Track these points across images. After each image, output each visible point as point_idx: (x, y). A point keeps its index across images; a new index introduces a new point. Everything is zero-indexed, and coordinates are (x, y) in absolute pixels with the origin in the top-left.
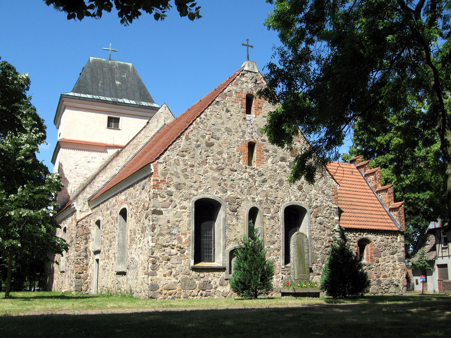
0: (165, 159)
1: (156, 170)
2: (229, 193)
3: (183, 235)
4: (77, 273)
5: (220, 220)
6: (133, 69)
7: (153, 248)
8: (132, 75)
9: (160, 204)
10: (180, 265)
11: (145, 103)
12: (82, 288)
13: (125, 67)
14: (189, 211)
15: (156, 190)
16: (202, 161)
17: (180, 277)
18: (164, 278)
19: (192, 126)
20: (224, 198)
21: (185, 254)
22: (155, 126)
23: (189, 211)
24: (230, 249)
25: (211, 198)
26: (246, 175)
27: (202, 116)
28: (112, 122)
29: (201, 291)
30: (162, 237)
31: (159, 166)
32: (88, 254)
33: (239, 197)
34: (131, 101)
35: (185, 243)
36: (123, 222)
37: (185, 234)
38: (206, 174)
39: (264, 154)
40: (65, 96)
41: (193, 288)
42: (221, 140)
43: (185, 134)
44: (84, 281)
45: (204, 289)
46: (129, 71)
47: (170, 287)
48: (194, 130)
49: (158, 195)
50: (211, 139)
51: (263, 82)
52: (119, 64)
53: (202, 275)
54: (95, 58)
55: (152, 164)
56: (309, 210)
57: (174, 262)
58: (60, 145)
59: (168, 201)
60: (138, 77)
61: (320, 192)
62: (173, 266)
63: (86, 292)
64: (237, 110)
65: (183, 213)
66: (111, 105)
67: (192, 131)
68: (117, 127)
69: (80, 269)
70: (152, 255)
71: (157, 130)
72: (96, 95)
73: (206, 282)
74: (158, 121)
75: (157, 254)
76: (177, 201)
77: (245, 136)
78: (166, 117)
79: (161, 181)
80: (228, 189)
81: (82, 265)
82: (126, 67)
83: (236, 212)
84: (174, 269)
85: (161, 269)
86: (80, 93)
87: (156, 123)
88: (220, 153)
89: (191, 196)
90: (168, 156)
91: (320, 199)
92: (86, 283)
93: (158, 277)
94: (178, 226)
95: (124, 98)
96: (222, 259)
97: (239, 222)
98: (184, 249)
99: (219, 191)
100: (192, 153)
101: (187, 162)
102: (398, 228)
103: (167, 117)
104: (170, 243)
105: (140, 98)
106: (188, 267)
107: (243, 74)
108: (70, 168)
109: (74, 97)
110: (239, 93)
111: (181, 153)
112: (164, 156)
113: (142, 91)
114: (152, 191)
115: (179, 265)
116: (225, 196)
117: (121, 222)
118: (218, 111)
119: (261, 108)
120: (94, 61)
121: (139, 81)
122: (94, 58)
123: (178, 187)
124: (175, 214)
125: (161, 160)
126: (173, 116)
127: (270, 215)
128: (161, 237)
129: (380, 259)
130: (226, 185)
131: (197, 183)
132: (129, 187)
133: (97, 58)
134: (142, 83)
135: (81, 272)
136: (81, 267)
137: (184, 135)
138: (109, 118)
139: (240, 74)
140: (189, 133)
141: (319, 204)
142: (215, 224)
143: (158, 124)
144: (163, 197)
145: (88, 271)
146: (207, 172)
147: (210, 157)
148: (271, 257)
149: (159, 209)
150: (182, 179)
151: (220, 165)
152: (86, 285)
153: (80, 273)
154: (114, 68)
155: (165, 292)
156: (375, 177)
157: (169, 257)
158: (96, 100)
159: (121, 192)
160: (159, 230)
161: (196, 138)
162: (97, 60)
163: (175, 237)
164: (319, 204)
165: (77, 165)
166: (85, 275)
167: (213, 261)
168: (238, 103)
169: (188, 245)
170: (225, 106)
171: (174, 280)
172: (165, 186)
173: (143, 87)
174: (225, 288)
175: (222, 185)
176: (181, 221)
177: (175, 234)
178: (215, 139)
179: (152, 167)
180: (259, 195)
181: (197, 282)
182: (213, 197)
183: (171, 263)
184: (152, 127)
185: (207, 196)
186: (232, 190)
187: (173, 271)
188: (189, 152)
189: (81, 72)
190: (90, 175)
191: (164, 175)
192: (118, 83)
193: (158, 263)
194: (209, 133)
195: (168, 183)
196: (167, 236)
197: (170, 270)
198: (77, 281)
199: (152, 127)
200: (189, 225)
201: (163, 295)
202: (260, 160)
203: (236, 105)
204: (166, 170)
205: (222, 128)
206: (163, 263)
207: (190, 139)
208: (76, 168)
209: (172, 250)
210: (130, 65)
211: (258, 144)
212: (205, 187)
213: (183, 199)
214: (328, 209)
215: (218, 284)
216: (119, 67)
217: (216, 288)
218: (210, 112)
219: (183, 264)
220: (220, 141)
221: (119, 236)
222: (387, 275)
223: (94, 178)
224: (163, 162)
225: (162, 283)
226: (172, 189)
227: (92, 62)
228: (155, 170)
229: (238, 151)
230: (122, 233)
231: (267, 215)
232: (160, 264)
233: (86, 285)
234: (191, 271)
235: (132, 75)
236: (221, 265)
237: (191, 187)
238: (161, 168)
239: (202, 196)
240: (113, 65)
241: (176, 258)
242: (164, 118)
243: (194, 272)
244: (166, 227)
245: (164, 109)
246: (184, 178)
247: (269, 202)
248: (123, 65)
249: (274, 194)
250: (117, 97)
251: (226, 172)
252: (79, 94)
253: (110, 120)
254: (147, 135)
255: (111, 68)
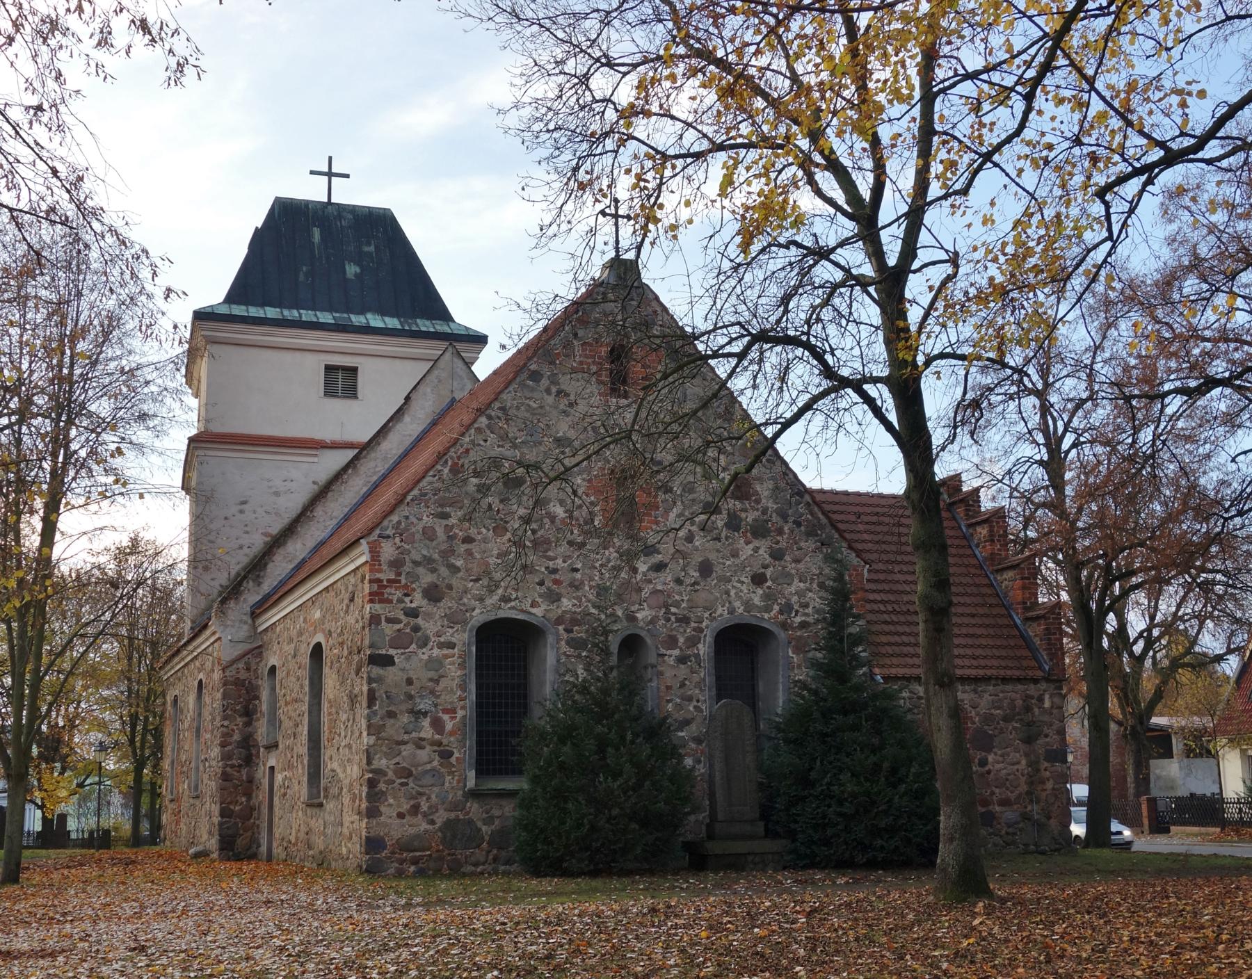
11: (428, 323)
15: (377, 606)
17: (441, 817)
18: (398, 821)
21: (453, 760)
32: (254, 752)
34: (387, 319)
35: (452, 733)
61: (815, 586)
65: (446, 656)
67: (467, 451)
68: (351, 392)
72: (290, 308)
75: (381, 762)
79: (389, 581)
95: (370, 310)
99: (539, 600)
102: (1044, 671)
110: (590, 345)
114: (368, 607)
116: (556, 612)
123: (433, 594)
127: (676, 652)
129: (991, 758)
138: (329, 369)
149: (384, 652)
156: (991, 531)
165: (244, 503)
172: (399, 594)
175: (548, 583)
185: (506, 612)
190: (275, 529)
193: (382, 786)
195: (406, 586)
200: (463, 687)
208: (241, 512)
209: (419, 752)
219: (447, 784)
222: (1012, 796)
223: (290, 531)
226: (418, 601)
231: (668, 652)
247: (673, 618)
250: (350, 310)
252: (244, 308)
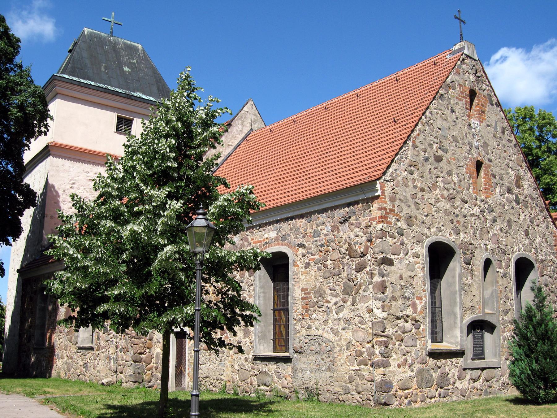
0: (392, 176)
1: (383, 192)
2: (462, 235)
3: (418, 300)
4: (136, 353)
5: (454, 277)
6: (144, 52)
7: (385, 321)
8: (143, 62)
9: (390, 247)
10: (415, 347)
12: (144, 377)
13: (132, 50)
14: (422, 262)
15: (385, 225)
16: (433, 183)
17: (416, 367)
19: (418, 127)
20: (458, 242)
21: (421, 330)
22: (239, 131)
23: (422, 262)
24: (467, 321)
25: (445, 242)
26: (476, 210)
27: (427, 113)
28: (122, 124)
29: (439, 389)
30: (395, 303)
31: (386, 185)
33: (472, 242)
35: (421, 313)
36: (264, 275)
37: (420, 298)
38: (438, 205)
39: (492, 181)
40: (59, 78)
41: (430, 385)
42: (450, 153)
43: (412, 139)
44: (147, 366)
45: (442, 385)
46: (139, 55)
47: (406, 384)
48: (421, 133)
49: (387, 233)
50: (439, 151)
51: (483, 75)
52: (124, 43)
53: (439, 363)
54: (92, 30)
55: (378, 182)
56: (536, 265)
57: (408, 344)
58: (49, 151)
59: (399, 244)
60: (152, 65)
62: (408, 349)
63: (150, 384)
64: (463, 112)
66: (124, 99)
67: (418, 135)
69: (141, 347)
70: (383, 332)
71: (242, 138)
73: (443, 374)
74: (242, 123)
76: (409, 244)
77: (472, 151)
78: (253, 120)
80: (462, 229)
81: (143, 340)
82: (135, 49)
83: (470, 264)
84: (409, 354)
85: (394, 356)
86: (74, 76)
87: (240, 126)
88: (450, 173)
89: (424, 237)
90: (396, 170)
91: (545, 250)
92: (150, 369)
93: (391, 368)
94: (411, 285)
95: (138, 91)
96: (459, 338)
97: (474, 281)
98: (419, 323)
99: (452, 232)
100: (420, 169)
101: (416, 182)
103: (254, 119)
104: (404, 313)
105: (159, 93)
106: (424, 351)
107: (463, 60)
108: (63, 186)
109: (73, 81)
111: (409, 168)
112: (390, 170)
113: (160, 84)
115: (414, 348)
117: (262, 275)
118: (443, 108)
119: (483, 112)
120: (91, 34)
121: (154, 71)
122: (89, 30)
123: (410, 220)
124: (408, 264)
125: (388, 177)
126: (261, 119)
128: (394, 303)
130: (458, 222)
131: (428, 217)
132: (301, 216)
133: (95, 31)
134: (159, 74)
135: (143, 351)
136: (143, 343)
137: (410, 139)
139: (461, 59)
140: (415, 137)
141: (544, 257)
142: (441, 283)
143: (242, 129)
144: (393, 237)
145: (153, 350)
146: (437, 201)
147: (440, 179)
148: (505, 334)
150: (412, 211)
151: (451, 191)
152: (150, 372)
153: (141, 353)
154: (119, 48)
155: (400, 393)
157: (403, 335)
158: (103, 90)
159: (270, 223)
160: (391, 291)
161: (423, 147)
162: (95, 33)
163: (410, 302)
164: (544, 257)
166: (149, 355)
167: (439, 340)
168: (462, 101)
169: (424, 315)
170: (450, 103)
171: (409, 373)
173: (160, 79)
174: (463, 383)
175: (455, 223)
176: (415, 277)
177: (409, 298)
178: (443, 151)
179: (378, 186)
180: (491, 241)
181: (434, 374)
182: (447, 241)
183: (405, 344)
184: (236, 133)
186: (465, 231)
187: (408, 358)
188: (417, 167)
189: (71, 48)
191: (393, 200)
192: (126, 69)
193: (390, 346)
194: (436, 140)
195: (397, 215)
196: (400, 302)
197: (404, 357)
198: (136, 366)
199: (236, 133)
201: (399, 399)
202: (489, 189)
203: (460, 103)
204: (394, 193)
205: (449, 136)
206: (397, 346)
207: (417, 147)
208: (71, 188)
209: (406, 324)
210: (140, 46)
211: (485, 164)
212: (437, 223)
213: (415, 241)
214: (552, 266)
215: (456, 377)
216: (125, 48)
217: (454, 383)
218: (435, 109)
219: (418, 346)
220: (449, 155)
221: (259, 297)
224: (390, 180)
225: (397, 378)
226: (402, 224)
227: (88, 35)
228: (382, 192)
229: (468, 173)
230: (264, 293)
232: (394, 347)
233: (150, 372)
234: (428, 358)
235: (143, 62)
236: (459, 348)
237: (423, 223)
238: (388, 187)
239: (436, 239)
240: (116, 43)
241: (411, 336)
242: (250, 121)
243: (431, 359)
244: (399, 287)
245: (251, 107)
246: (415, 209)
248: (129, 45)
249: (504, 240)
251: (458, 203)
253: (120, 120)
254: (230, 144)
255: (114, 46)
